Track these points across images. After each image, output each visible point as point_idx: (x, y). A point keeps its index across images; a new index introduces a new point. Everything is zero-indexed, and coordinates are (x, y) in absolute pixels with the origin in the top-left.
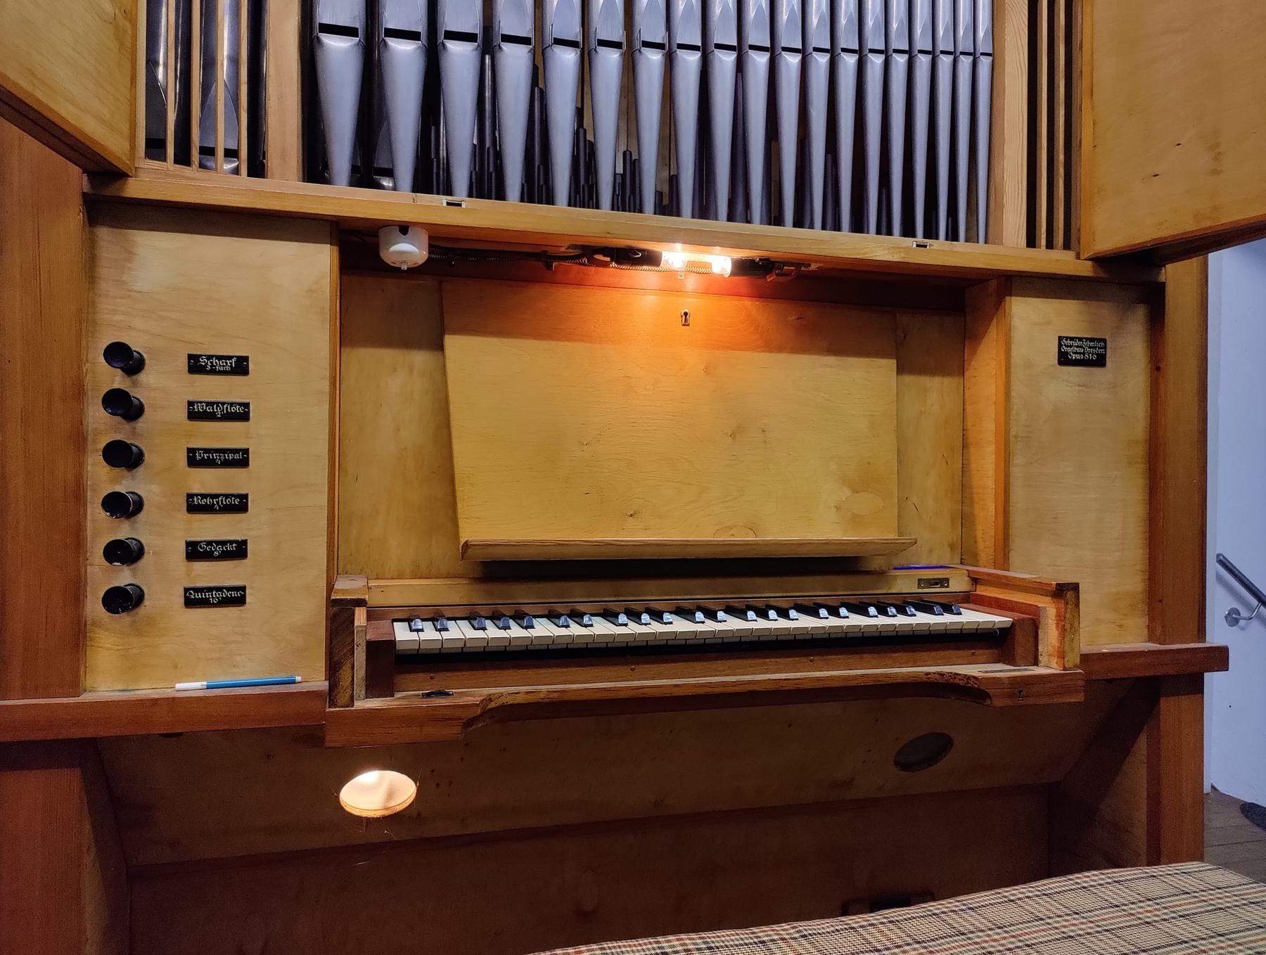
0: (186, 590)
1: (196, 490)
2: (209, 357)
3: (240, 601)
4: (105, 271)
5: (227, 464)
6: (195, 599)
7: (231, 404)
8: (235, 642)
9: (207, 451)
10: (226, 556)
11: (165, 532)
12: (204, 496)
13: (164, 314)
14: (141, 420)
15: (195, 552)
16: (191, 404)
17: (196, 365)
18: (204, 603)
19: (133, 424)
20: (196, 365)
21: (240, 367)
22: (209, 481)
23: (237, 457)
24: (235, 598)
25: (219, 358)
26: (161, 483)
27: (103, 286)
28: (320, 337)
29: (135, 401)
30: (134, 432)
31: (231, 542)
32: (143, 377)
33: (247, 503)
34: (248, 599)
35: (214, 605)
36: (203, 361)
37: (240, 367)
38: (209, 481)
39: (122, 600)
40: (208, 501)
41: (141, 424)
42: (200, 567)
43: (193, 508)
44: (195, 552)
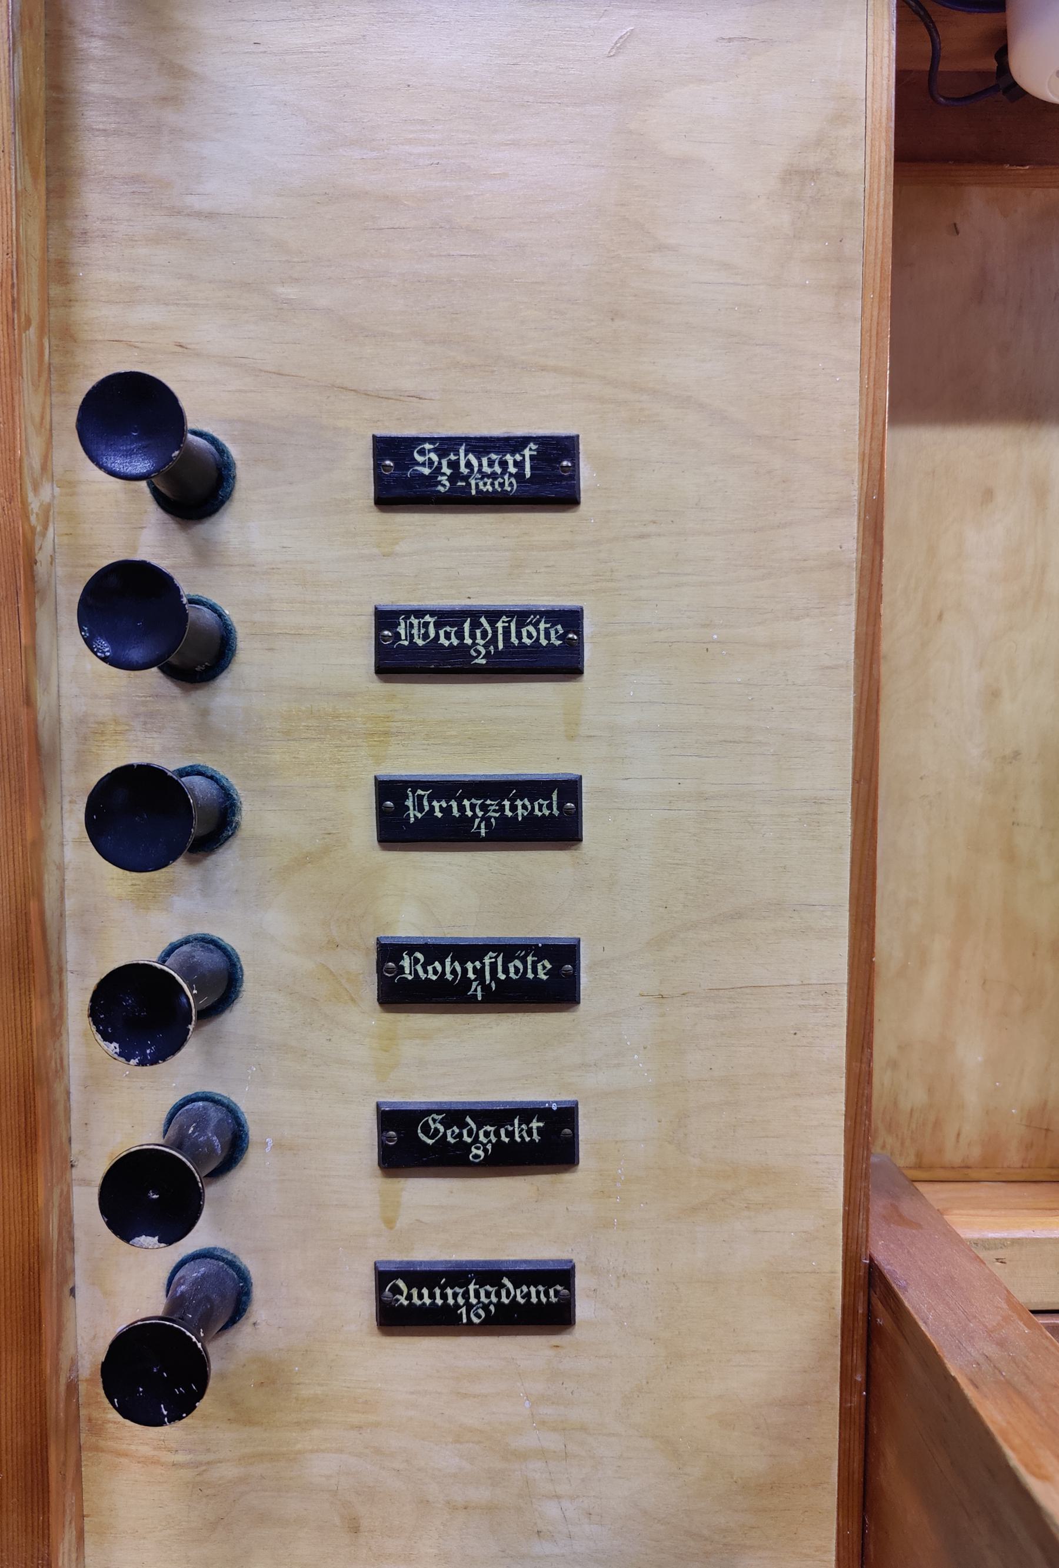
0: (384, 1277)
1: (408, 926)
2: (446, 445)
3: (558, 1317)
4: (103, 148)
5: (510, 834)
6: (416, 1302)
7: (522, 616)
8: (542, 1454)
9: (443, 789)
10: (508, 1159)
11: (310, 1071)
12: (435, 951)
13: (289, 292)
14: (225, 682)
15: (410, 1143)
16: (385, 619)
17: (407, 478)
18: (441, 1320)
19: (201, 696)
20: (407, 478)
21: (548, 476)
22: (453, 895)
23: (541, 809)
24: (536, 1302)
25: (481, 445)
26: (298, 901)
27: (96, 202)
28: (828, 351)
29: (200, 616)
30: (204, 728)
31: (526, 1113)
32: (230, 526)
33: (574, 980)
34: (582, 1309)
35: (471, 1329)
36: (424, 462)
37: (548, 476)
38: (453, 895)
39: (157, 1372)
40: (449, 967)
41: (226, 694)
42: (427, 1194)
43: (398, 993)
44: (410, 1143)
